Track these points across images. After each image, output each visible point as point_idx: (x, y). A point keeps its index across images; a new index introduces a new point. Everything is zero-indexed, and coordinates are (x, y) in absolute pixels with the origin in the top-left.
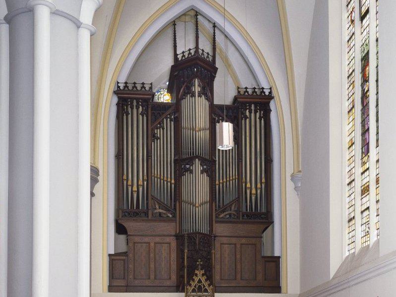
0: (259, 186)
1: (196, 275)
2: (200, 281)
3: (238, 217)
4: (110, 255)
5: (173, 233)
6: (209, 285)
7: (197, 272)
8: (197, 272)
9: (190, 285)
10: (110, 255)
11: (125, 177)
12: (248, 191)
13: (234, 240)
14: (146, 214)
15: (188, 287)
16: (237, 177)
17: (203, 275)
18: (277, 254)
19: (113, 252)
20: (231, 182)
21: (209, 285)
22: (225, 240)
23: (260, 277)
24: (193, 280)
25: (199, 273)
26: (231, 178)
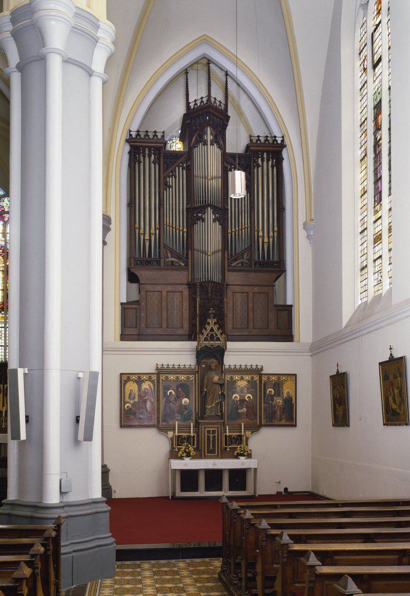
0: (271, 234)
1: (209, 324)
2: (212, 330)
3: (250, 266)
4: (122, 304)
5: (186, 282)
6: (221, 334)
7: (209, 320)
8: (209, 320)
9: (203, 334)
10: (122, 304)
11: (137, 226)
12: (261, 240)
13: (246, 289)
14: (159, 263)
15: (201, 336)
16: (249, 225)
17: (215, 324)
18: (289, 303)
19: (125, 301)
20: (243, 230)
21: (221, 334)
22: (237, 289)
23: (272, 325)
24: (206, 329)
25: (212, 321)
26: (243, 227)
